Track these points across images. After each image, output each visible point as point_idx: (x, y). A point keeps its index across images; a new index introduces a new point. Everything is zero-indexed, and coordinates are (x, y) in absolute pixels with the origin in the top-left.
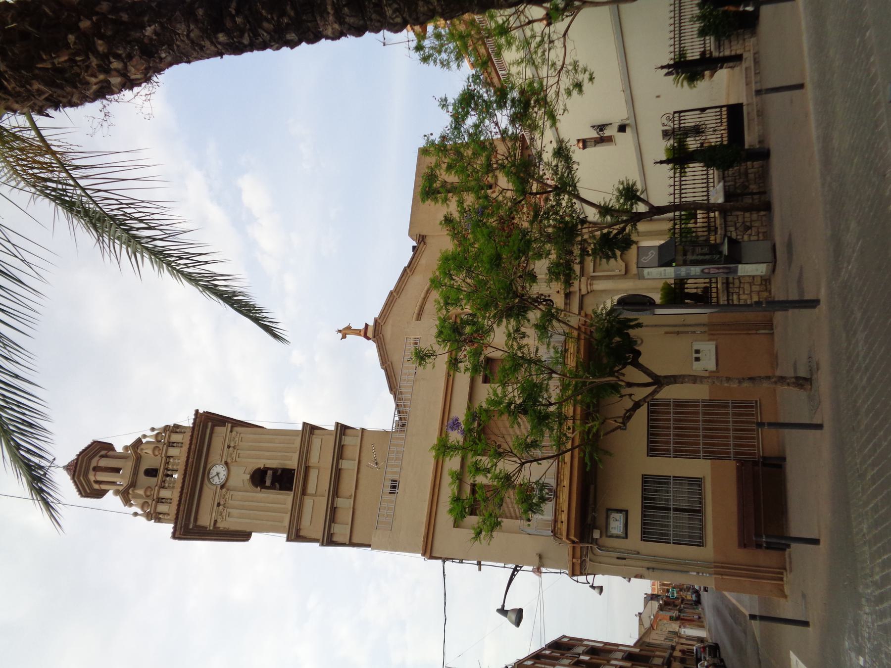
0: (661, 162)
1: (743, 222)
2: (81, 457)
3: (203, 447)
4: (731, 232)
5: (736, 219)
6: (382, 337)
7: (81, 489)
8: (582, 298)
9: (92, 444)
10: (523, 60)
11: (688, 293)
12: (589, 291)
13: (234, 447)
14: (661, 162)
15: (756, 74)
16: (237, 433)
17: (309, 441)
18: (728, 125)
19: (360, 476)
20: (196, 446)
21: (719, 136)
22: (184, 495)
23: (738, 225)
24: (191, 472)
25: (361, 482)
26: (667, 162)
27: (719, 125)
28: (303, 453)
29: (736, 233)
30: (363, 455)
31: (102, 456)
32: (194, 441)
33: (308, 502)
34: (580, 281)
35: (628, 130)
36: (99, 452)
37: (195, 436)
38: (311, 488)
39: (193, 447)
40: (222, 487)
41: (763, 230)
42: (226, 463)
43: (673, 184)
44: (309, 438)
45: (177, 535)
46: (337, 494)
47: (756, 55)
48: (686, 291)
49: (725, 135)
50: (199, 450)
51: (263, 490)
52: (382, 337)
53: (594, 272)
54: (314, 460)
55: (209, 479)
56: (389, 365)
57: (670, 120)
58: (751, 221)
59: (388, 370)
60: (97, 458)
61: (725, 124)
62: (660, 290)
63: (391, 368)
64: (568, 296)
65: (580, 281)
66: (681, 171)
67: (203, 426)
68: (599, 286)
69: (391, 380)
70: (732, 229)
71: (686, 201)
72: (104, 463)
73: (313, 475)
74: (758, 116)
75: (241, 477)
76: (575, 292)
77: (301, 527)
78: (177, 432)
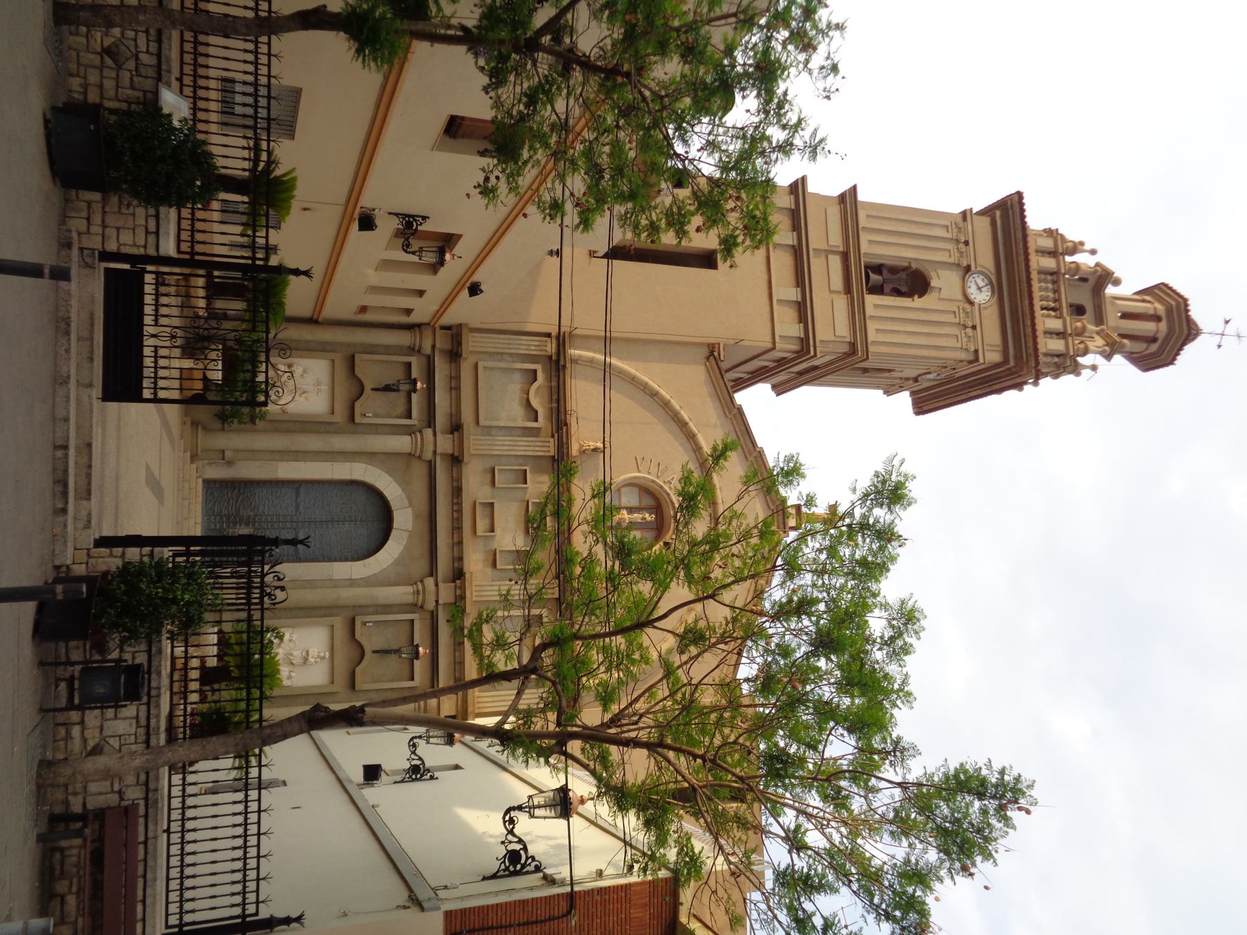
0: (297, 272)
1: (119, 67)
2: (1186, 332)
3: (1013, 328)
4: (148, 52)
5: (135, 79)
6: (770, 504)
7: (1169, 291)
8: (432, 572)
9: (1174, 359)
10: (606, 768)
11: (243, 194)
12: (419, 584)
13: (965, 327)
14: (297, 272)
15: (66, 448)
16: (966, 349)
17: (855, 332)
18: (141, 346)
19: (765, 277)
20: (1024, 326)
21: (163, 321)
22: (1021, 252)
23: (131, 64)
24: (1020, 286)
25: (763, 268)
26: (281, 270)
27: (162, 352)
28: (859, 312)
29: (136, 46)
30: (768, 309)
31: (1154, 340)
32: (1029, 330)
33: (836, 240)
34: (437, 602)
35: (359, 776)
36: (1160, 347)
37: (1030, 339)
38: (836, 262)
39: (1029, 323)
40: (968, 269)
41: (77, 39)
42: (971, 303)
43: (261, 905)
44: (855, 338)
45: (1016, 198)
46: (796, 251)
47: (60, 505)
48: (246, 199)
49: (148, 320)
50: (1018, 321)
51: (906, 264)
52: (770, 504)
53: (412, 621)
54: (841, 303)
55: (991, 283)
56: (751, 455)
57: (274, 385)
58: (102, 67)
59: (750, 445)
60: (1161, 336)
61: (147, 351)
62: (297, 198)
63: (746, 450)
64: (458, 575)
65: (437, 602)
66: (248, 717)
67: (1022, 357)
68: (402, 593)
69: (743, 428)
70: (144, 58)
71: (246, 40)
72: (1148, 327)
73: (837, 281)
74: (67, 321)
75: (945, 282)
76: (445, 581)
77: (838, 207)
78: (1058, 356)
